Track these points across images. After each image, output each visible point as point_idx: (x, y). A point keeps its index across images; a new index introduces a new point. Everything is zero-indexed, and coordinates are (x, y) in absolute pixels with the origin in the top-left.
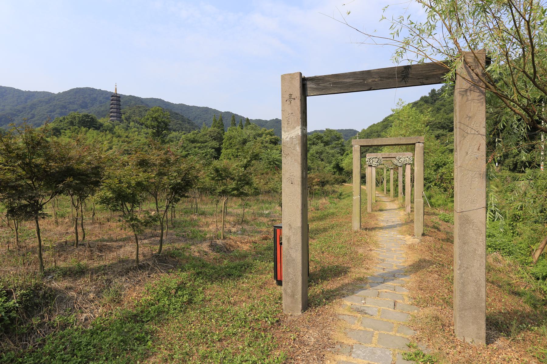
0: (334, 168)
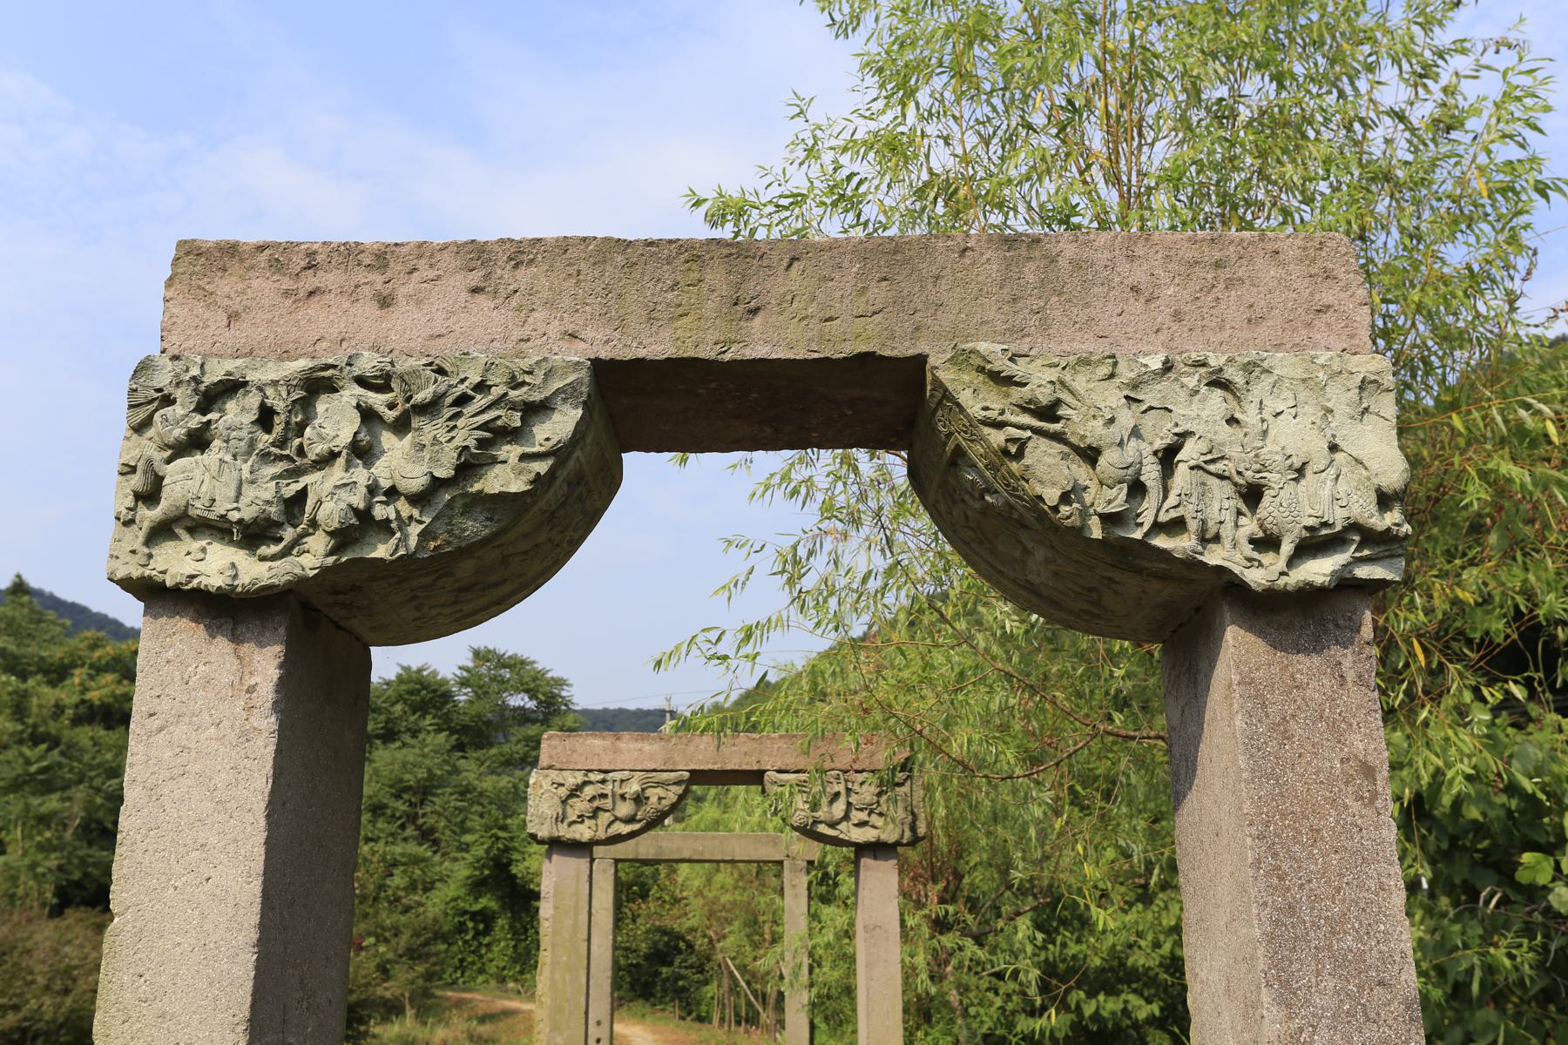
0: (477, 886)
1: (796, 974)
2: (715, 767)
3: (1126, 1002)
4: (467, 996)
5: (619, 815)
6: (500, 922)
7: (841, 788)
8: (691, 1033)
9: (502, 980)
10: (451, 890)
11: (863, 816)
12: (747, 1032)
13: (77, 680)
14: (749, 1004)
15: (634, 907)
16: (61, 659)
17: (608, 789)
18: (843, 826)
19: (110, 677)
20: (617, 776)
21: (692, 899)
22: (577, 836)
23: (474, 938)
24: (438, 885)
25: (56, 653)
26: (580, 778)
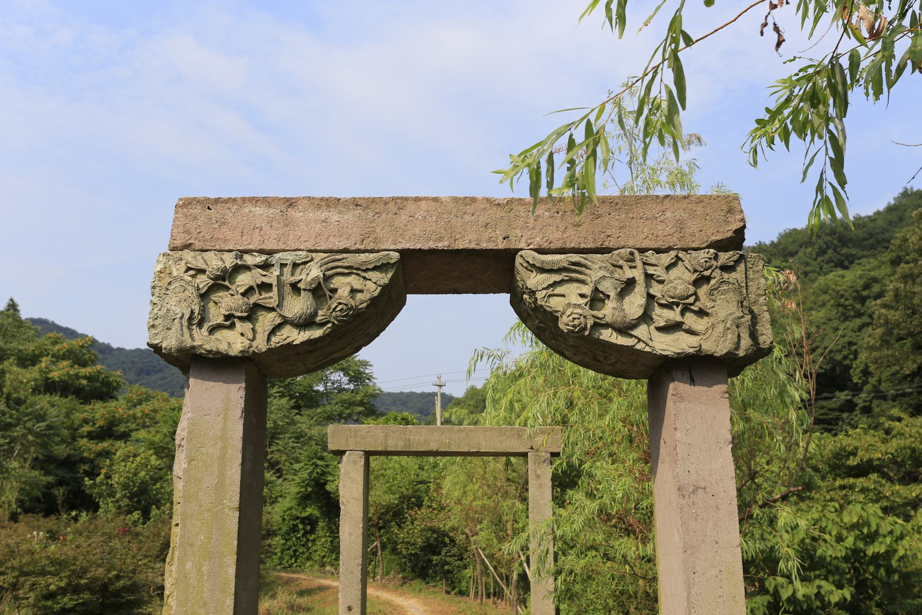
0: (304, 499)
1: (542, 561)
2: (440, 246)
3: (819, 587)
4: (295, 576)
5: (289, 315)
6: (321, 524)
7: (637, 274)
8: (457, 604)
9: (323, 565)
10: (286, 503)
11: (674, 315)
12: (495, 603)
13: (43, 365)
14: (496, 582)
15: (413, 513)
16: (33, 351)
17: (272, 277)
18: (642, 331)
19: (65, 363)
20: (289, 257)
21: (452, 504)
22: (223, 347)
23: (303, 535)
24: (280, 499)
25: (30, 347)
26: (229, 261)
